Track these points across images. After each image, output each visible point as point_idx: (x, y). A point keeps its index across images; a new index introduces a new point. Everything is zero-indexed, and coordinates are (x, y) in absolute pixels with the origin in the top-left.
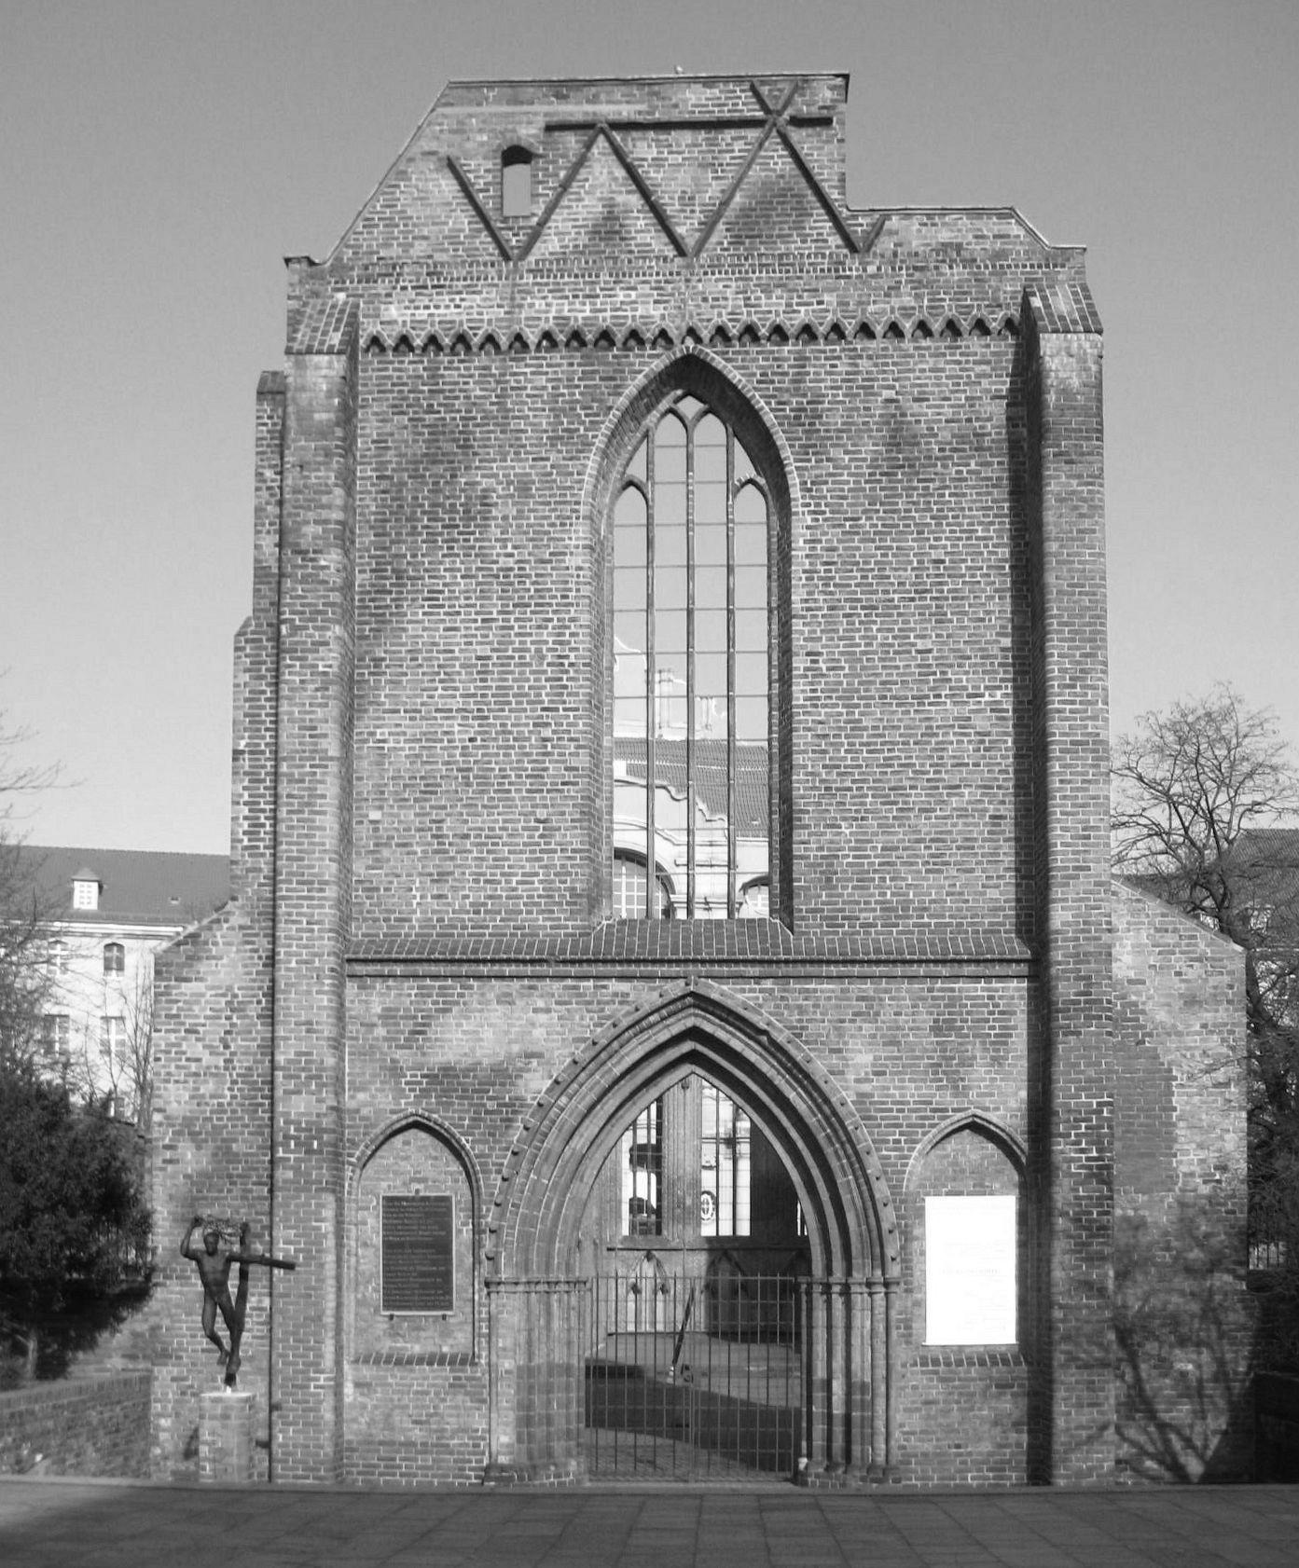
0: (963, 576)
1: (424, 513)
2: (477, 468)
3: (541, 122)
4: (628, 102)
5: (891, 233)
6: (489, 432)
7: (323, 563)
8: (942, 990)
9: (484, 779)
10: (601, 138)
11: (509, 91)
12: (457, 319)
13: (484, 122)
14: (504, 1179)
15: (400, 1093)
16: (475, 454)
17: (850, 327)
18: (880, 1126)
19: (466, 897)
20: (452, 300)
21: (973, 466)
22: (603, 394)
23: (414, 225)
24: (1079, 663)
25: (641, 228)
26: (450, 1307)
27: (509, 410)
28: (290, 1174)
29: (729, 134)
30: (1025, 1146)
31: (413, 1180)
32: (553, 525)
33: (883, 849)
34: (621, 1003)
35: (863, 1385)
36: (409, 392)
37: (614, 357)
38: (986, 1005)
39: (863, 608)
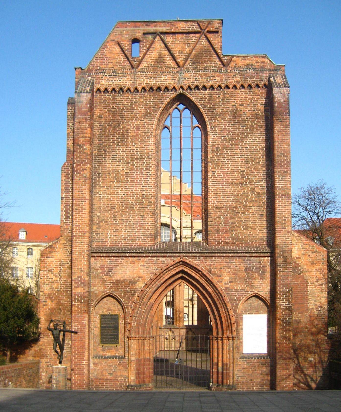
0: (253, 151)
1: (111, 135)
2: (125, 123)
3: (142, 32)
4: (165, 27)
5: (234, 61)
6: (128, 113)
7: (85, 148)
8: (247, 260)
9: (127, 205)
10: (158, 36)
11: (134, 24)
12: (120, 84)
13: (127, 32)
14: (132, 310)
15: (105, 287)
16: (125, 119)
17: (223, 86)
18: (231, 296)
19: (122, 236)
20: (119, 79)
21: (255, 123)
22: (158, 103)
23: (109, 59)
24: (283, 174)
25: (168, 60)
26: (118, 343)
27: (134, 108)
28: (76, 309)
29: (191, 35)
30: (269, 301)
31: (108, 310)
32: (145, 138)
33: (232, 223)
34: (163, 264)
35: (227, 364)
36: (107, 103)
37: (161, 94)
38: (259, 264)
39: (227, 160)
